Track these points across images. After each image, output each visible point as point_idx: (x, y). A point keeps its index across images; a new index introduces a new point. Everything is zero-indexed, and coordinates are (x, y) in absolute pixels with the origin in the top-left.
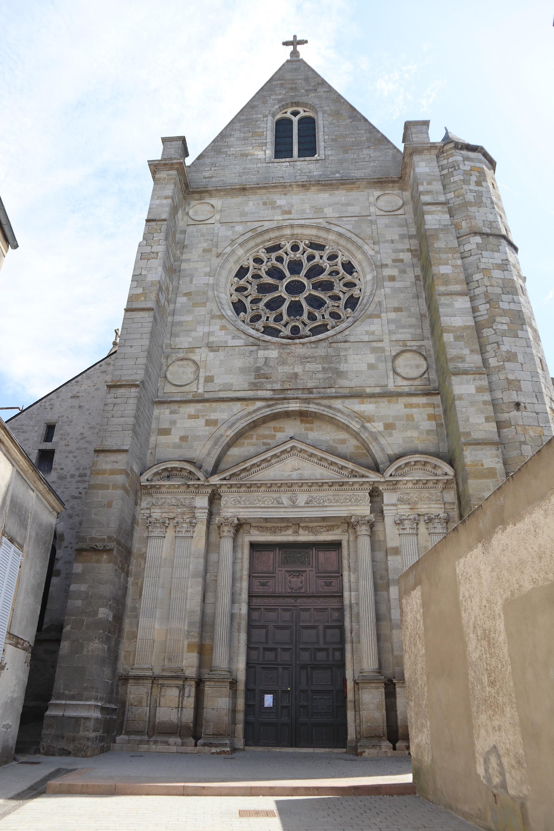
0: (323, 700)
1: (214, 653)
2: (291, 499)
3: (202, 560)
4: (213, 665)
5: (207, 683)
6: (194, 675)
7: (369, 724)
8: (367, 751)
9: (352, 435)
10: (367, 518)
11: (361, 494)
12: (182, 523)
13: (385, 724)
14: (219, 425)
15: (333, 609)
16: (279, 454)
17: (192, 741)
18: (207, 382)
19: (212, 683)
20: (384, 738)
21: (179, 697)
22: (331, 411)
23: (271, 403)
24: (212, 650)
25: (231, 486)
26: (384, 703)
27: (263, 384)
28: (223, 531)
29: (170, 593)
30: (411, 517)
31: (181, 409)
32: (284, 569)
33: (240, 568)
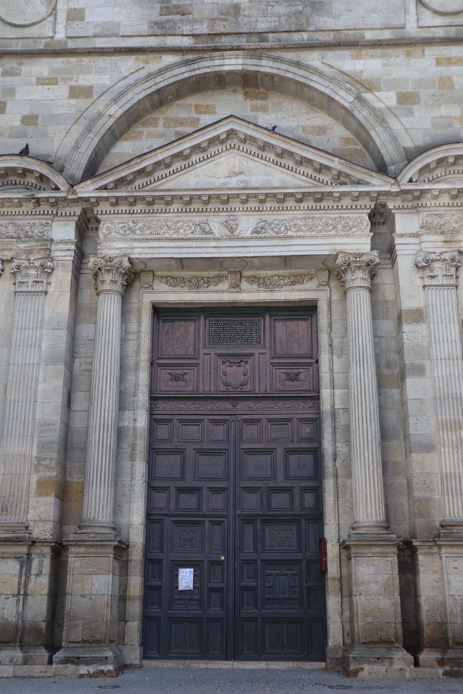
0: (282, 577)
1: (86, 497)
2: (226, 225)
3: (64, 334)
4: (84, 517)
5: (72, 550)
6: (48, 537)
7: (370, 620)
8: (367, 667)
9: (337, 118)
10: (365, 258)
11: (356, 216)
12: (26, 268)
13: (399, 620)
14: (95, 97)
15: (300, 420)
16: (205, 145)
17: (44, 653)
18: (72, 20)
19: (82, 550)
20: (397, 645)
21: (20, 577)
22: (301, 72)
23: (190, 57)
24: (82, 492)
25: (117, 202)
26: (397, 582)
27: (175, 24)
28: (103, 282)
29: (5, 392)
30: (446, 256)
31: (23, 68)
32: (213, 352)
33: (135, 349)
